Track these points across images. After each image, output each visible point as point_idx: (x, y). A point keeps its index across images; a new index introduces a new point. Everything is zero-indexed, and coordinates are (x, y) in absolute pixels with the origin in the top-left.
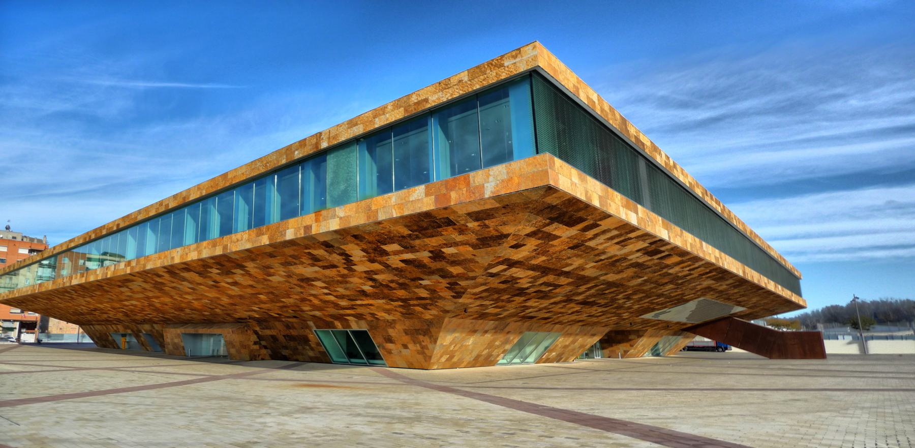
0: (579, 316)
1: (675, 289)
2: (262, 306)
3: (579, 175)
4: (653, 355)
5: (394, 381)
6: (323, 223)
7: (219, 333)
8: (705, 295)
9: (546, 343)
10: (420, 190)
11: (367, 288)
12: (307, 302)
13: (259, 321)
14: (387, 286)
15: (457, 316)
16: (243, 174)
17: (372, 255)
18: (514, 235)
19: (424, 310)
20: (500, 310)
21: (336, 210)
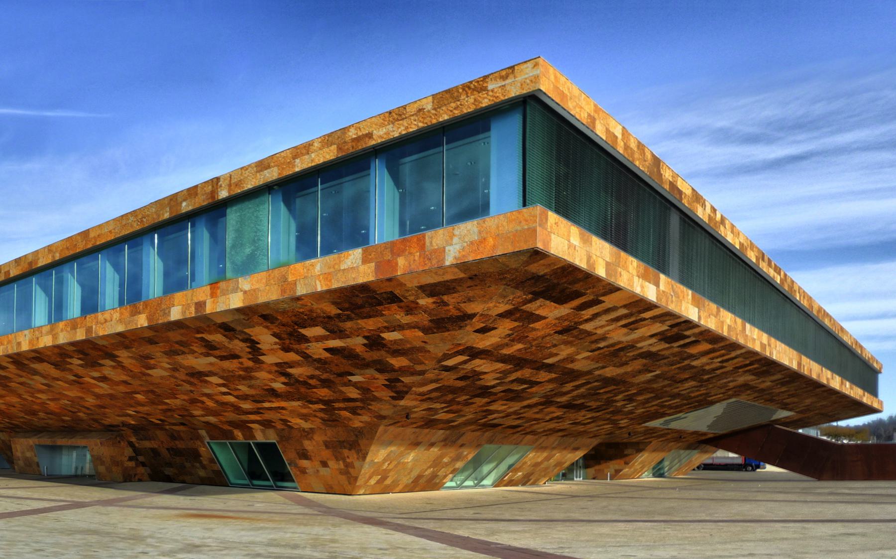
0: (560, 424)
1: (697, 387)
2: (140, 409)
3: (580, 234)
4: (654, 475)
5: (307, 511)
6: (222, 299)
7: (83, 445)
8: (738, 395)
9: (510, 460)
10: (354, 256)
11: (278, 386)
12: (198, 404)
13: (136, 429)
14: (305, 383)
15: (395, 423)
16: (110, 232)
17: (287, 342)
18: (482, 315)
19: (352, 416)
20: (454, 415)
21: (240, 280)
